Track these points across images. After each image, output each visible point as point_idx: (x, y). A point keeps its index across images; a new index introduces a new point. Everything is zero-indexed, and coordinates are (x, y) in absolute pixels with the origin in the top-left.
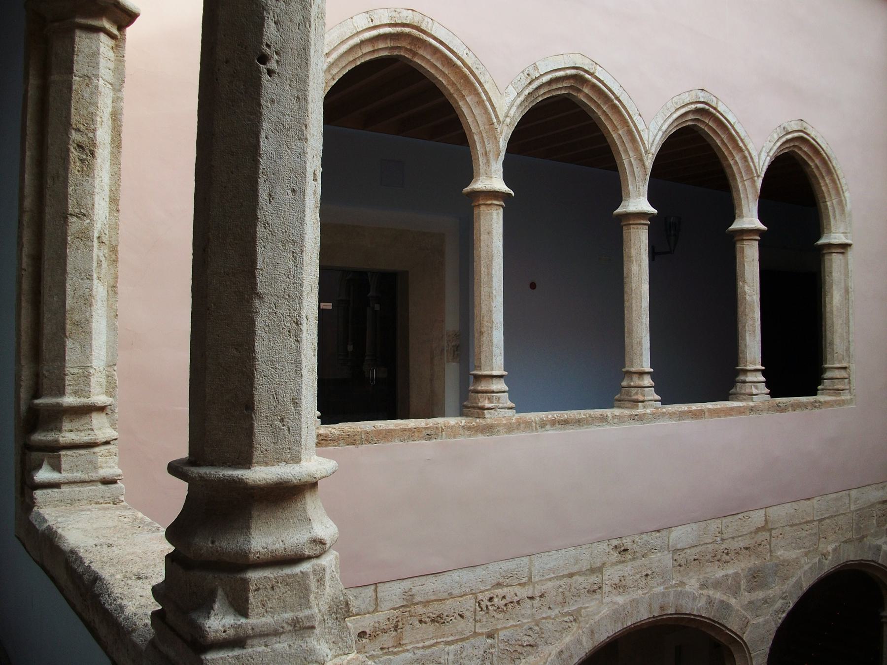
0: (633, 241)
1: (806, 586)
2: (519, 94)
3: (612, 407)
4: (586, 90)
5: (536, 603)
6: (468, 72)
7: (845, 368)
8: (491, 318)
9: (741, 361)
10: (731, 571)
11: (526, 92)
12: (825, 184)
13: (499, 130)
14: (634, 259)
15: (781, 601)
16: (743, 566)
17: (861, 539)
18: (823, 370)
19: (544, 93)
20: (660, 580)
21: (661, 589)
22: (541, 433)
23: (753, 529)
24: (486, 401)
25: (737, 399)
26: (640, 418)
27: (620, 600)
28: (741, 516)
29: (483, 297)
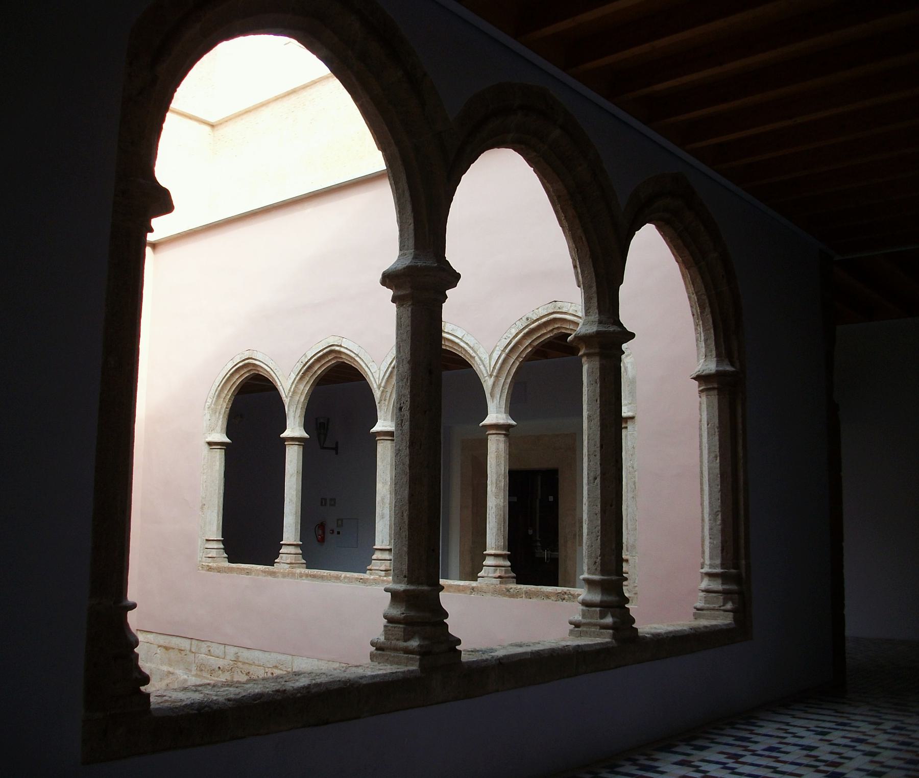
26: (364, 581)
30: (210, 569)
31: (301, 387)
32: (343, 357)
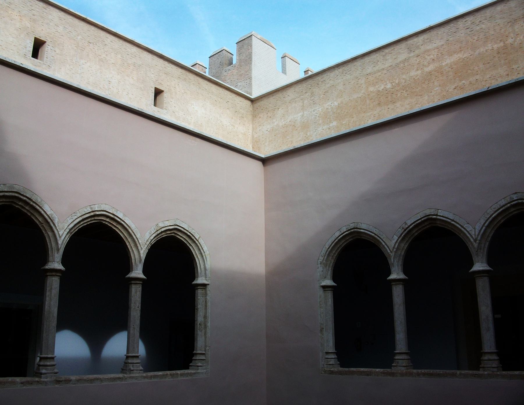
7: (204, 354)
26: (480, 376)
30: (332, 372)
31: (402, 245)
32: (438, 222)
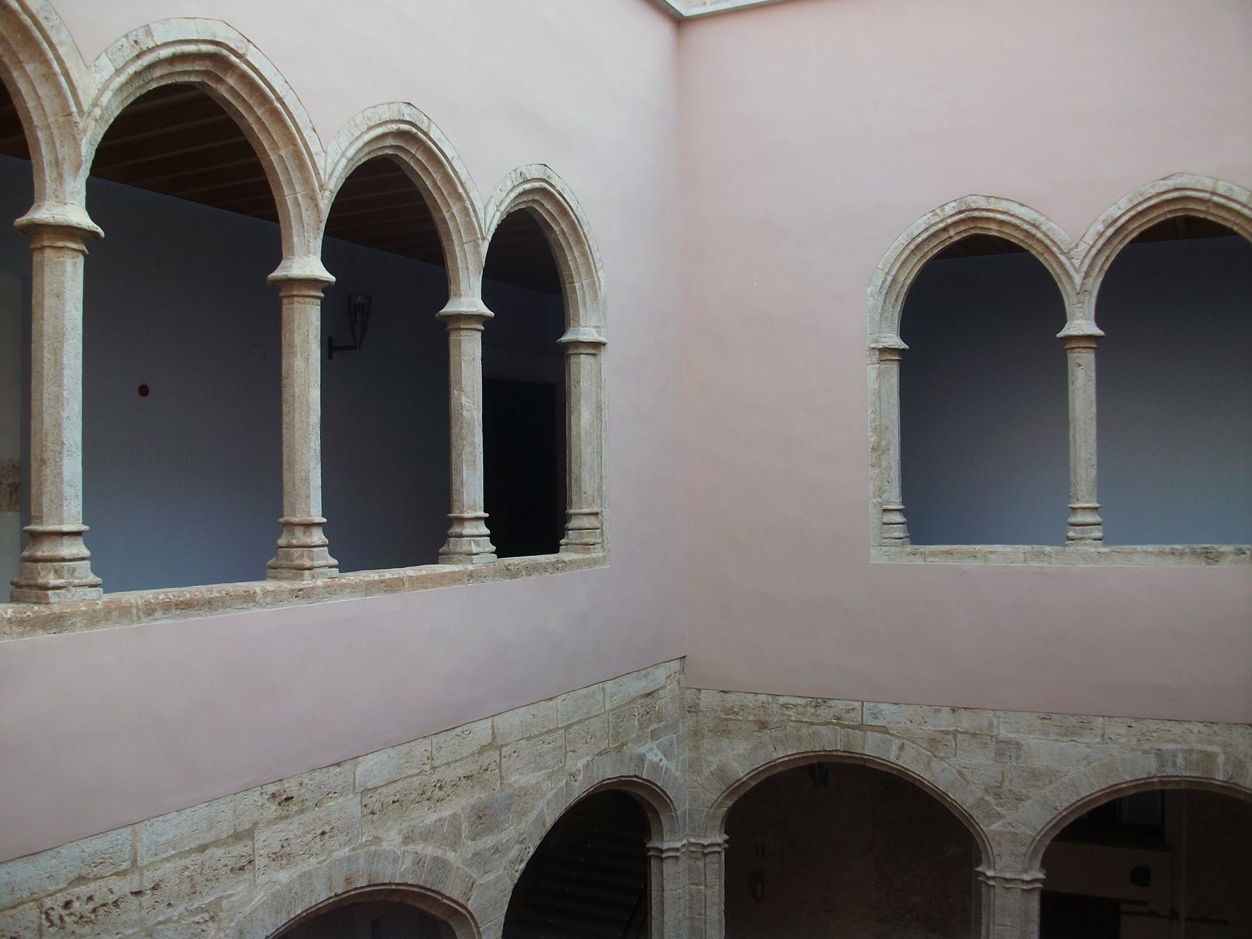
0: (296, 323)
1: (550, 822)
2: (118, 72)
3: (263, 577)
4: (231, 81)
5: (147, 899)
6: (29, 22)
7: (596, 514)
8: (59, 436)
9: (455, 505)
10: (446, 813)
11: (132, 70)
12: (573, 259)
13: (81, 126)
14: (298, 349)
15: (517, 846)
16: (463, 803)
17: (620, 748)
18: (567, 518)
19: (162, 77)
20: (342, 838)
21: (346, 851)
22: (147, 623)
23: (476, 748)
24: (52, 575)
25: (450, 562)
27: (284, 876)
28: (458, 731)
29: (46, 402)
